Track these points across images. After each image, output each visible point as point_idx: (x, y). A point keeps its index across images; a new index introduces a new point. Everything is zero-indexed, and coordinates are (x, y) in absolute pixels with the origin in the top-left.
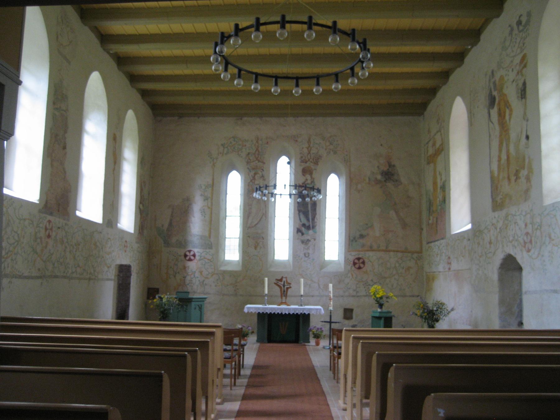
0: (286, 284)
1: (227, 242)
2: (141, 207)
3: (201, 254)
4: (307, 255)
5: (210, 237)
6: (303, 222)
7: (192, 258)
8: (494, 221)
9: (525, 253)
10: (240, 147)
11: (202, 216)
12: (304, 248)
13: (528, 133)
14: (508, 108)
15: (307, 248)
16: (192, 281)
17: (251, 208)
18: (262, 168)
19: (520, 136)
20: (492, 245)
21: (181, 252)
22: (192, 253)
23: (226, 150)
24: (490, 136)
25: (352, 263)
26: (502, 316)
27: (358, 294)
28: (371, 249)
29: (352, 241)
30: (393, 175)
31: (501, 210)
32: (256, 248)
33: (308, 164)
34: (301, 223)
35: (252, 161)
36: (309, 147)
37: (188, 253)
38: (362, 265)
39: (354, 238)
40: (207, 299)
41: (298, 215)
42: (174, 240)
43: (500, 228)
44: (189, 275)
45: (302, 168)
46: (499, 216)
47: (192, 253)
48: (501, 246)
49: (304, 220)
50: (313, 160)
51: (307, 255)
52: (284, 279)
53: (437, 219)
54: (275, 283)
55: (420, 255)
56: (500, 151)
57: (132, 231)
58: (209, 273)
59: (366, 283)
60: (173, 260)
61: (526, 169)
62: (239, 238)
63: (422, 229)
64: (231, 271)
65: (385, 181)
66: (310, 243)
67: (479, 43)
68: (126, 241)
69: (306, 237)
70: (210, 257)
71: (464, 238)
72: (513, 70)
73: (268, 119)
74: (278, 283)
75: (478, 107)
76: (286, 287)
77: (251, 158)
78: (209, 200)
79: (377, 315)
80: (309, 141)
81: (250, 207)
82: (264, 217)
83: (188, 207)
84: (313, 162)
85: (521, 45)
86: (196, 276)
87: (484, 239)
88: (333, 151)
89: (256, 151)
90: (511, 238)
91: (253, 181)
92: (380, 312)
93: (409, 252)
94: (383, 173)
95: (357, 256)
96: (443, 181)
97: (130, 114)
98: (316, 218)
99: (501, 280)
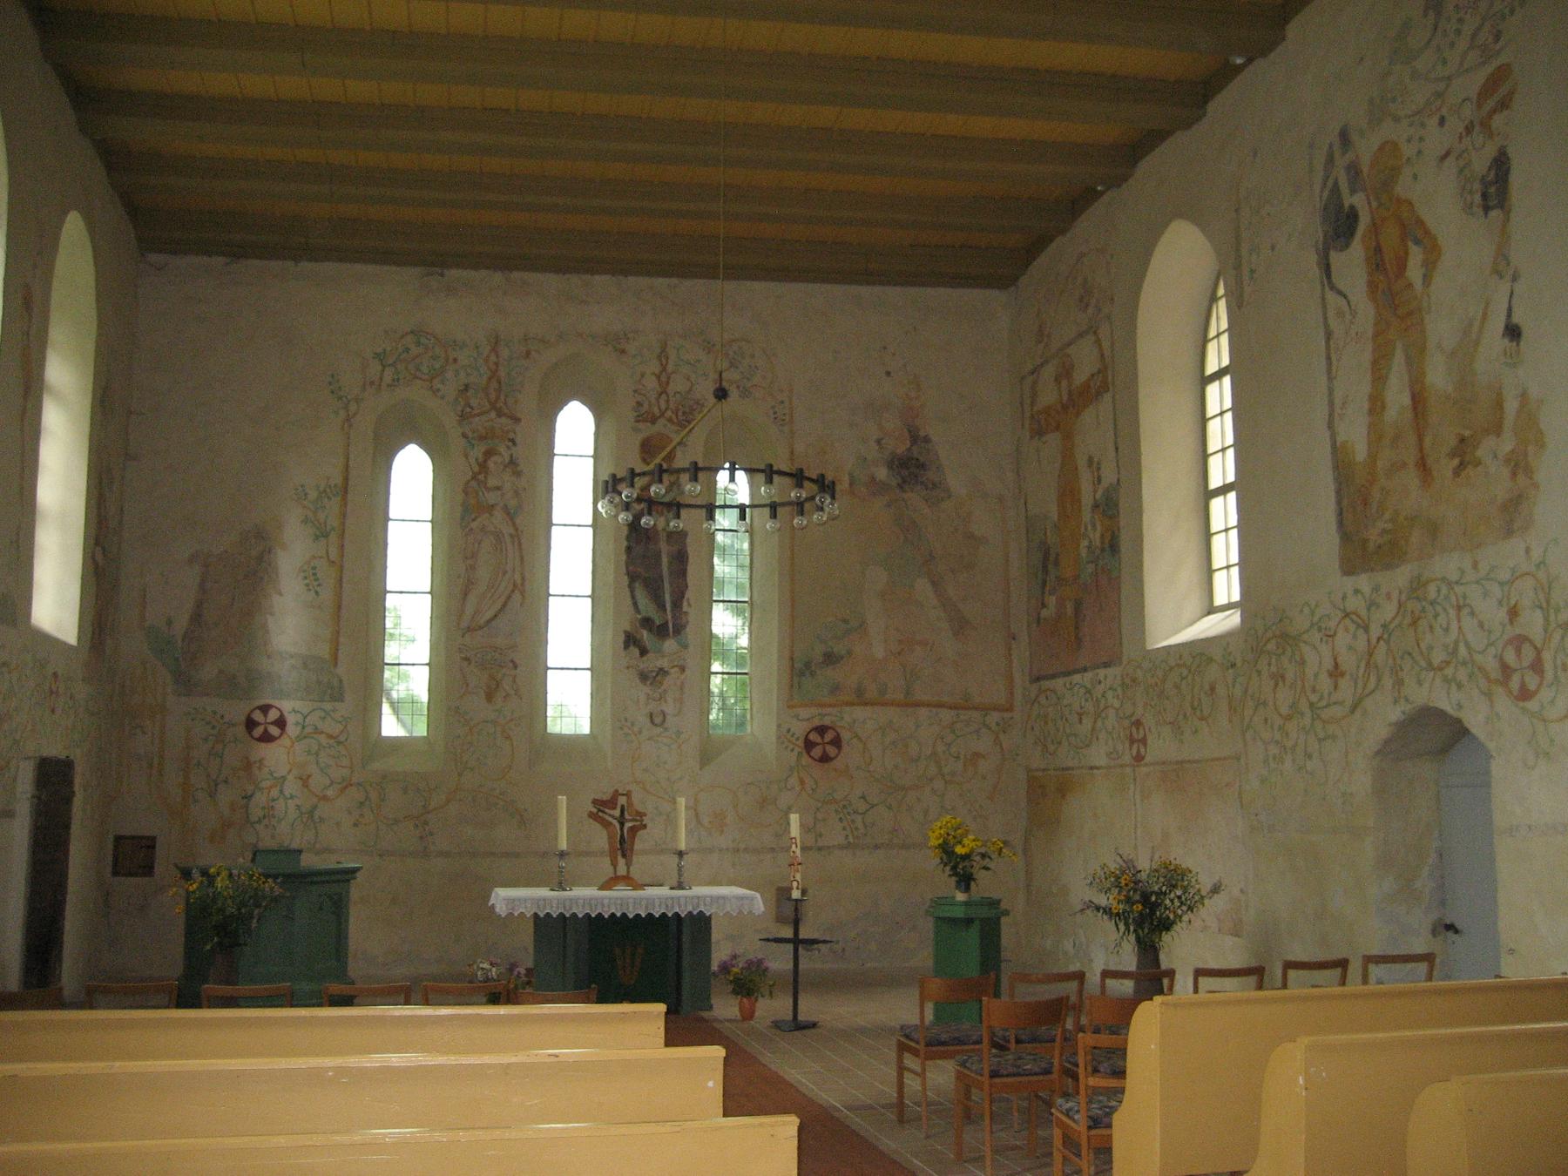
0: (627, 816)
2: (99, 558)
3: (305, 717)
6: (644, 614)
7: (274, 731)
8: (1354, 603)
9: (1503, 704)
13: (1515, 319)
14: (1417, 242)
15: (657, 695)
17: (473, 568)
18: (511, 435)
19: (1475, 328)
20: (1344, 683)
21: (237, 711)
22: (273, 715)
24: (1329, 335)
25: (801, 743)
27: (820, 844)
28: (861, 699)
31: (1388, 567)
32: (490, 697)
33: (659, 427)
34: (639, 617)
35: (476, 412)
36: (661, 373)
37: (258, 716)
38: (831, 750)
39: (807, 665)
40: (358, 875)
42: (208, 671)
44: (261, 789)
45: (640, 437)
46: (1376, 589)
47: (273, 715)
49: (647, 607)
50: (677, 415)
51: (656, 720)
52: (622, 800)
53: (1078, 605)
54: (591, 815)
55: (1007, 715)
56: (1379, 377)
57: (70, 634)
61: (1507, 434)
65: (900, 486)
66: (668, 682)
68: (55, 675)
69: (652, 663)
70: (335, 729)
71: (1211, 660)
72: (1442, 121)
76: (628, 825)
77: (474, 402)
78: (333, 537)
79: (959, 913)
80: (663, 355)
81: (469, 562)
82: (517, 596)
83: (260, 559)
86: (287, 794)
88: (738, 387)
92: (966, 904)
95: (817, 722)
96: (1105, 483)
97: (74, 228)
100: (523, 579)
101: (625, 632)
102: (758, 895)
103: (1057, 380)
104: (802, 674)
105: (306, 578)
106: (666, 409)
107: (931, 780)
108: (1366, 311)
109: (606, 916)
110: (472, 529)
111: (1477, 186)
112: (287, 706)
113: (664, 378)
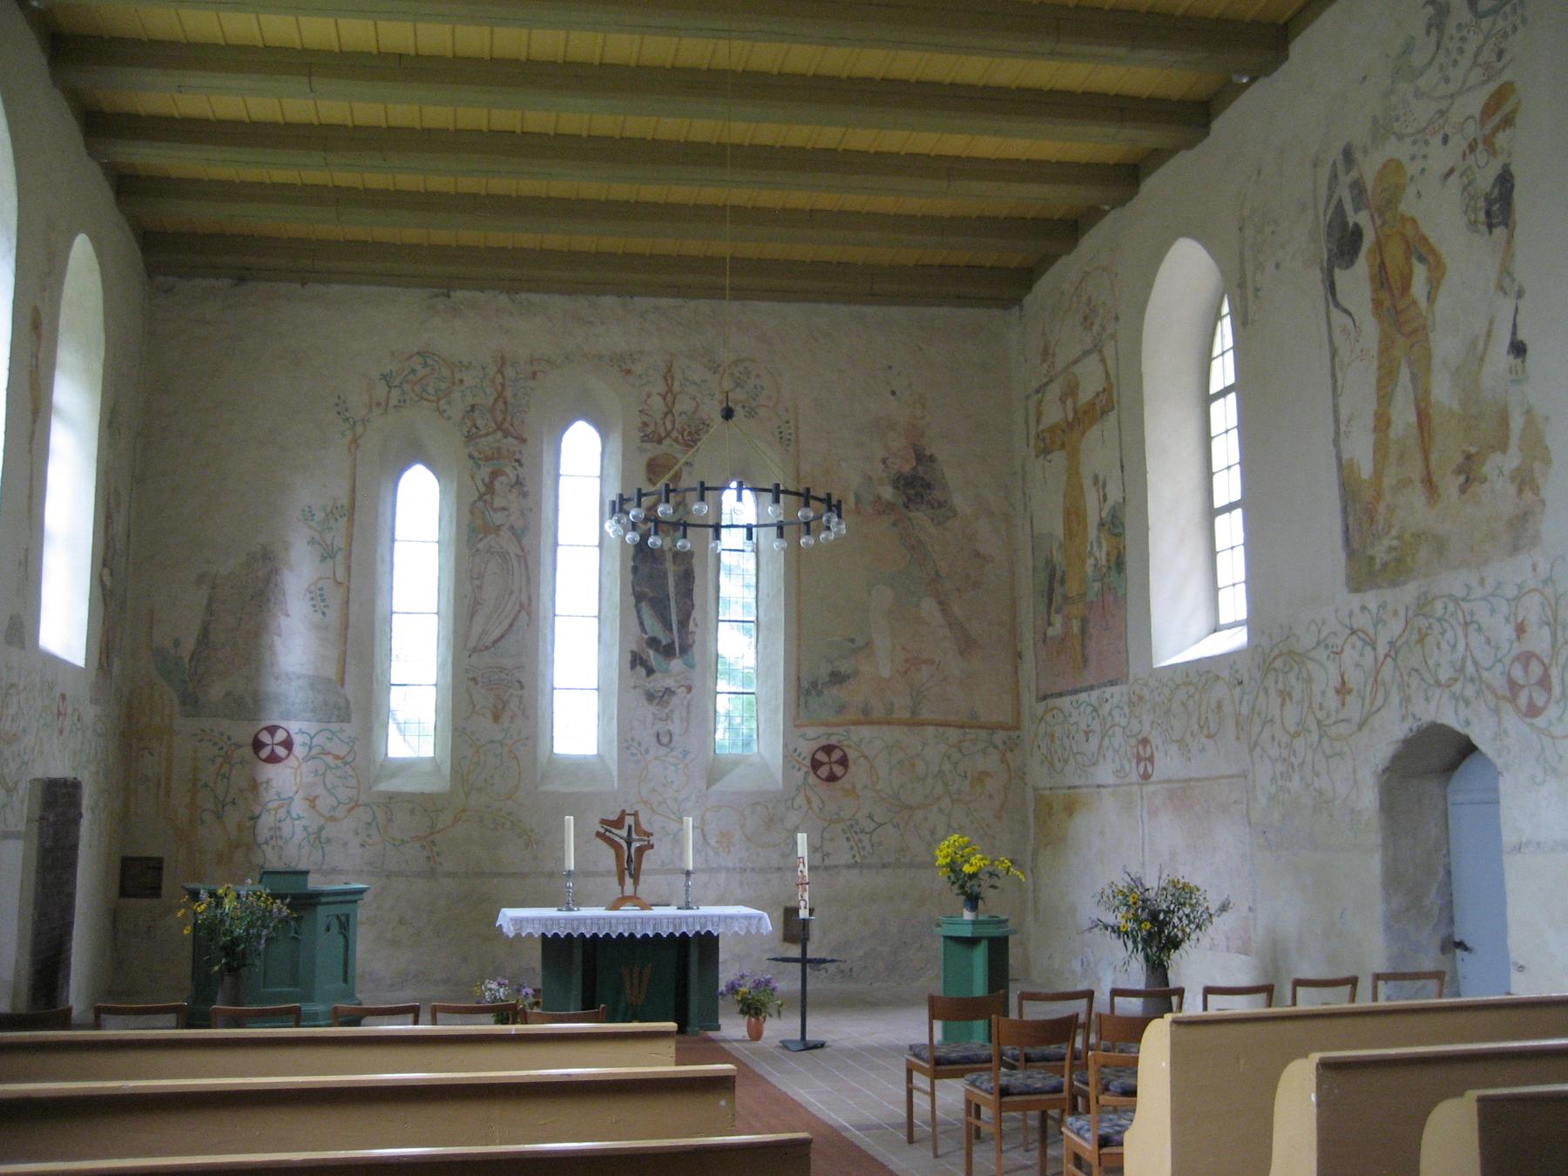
0: (634, 836)
1: (396, 698)
2: (107, 579)
4: (663, 739)
5: (342, 683)
6: (650, 634)
7: (281, 751)
8: (1361, 621)
9: (1511, 721)
10: (444, 386)
11: (316, 611)
12: (654, 715)
13: (1521, 336)
14: (1422, 259)
15: (663, 716)
16: (279, 828)
17: (480, 587)
18: (517, 456)
19: (1481, 346)
20: (1351, 700)
21: (243, 733)
22: (280, 736)
23: (395, 393)
24: (1334, 353)
25: (808, 762)
26: (1394, 924)
27: (827, 862)
28: (866, 718)
29: (808, 692)
30: (928, 486)
32: (496, 717)
33: (666, 446)
34: (646, 637)
37: (265, 737)
38: (838, 770)
39: (814, 685)
41: (634, 610)
42: (216, 692)
43: (1391, 644)
46: (1383, 606)
47: (280, 736)
48: (1395, 699)
49: (654, 628)
52: (629, 820)
54: (598, 834)
55: (1014, 734)
58: (339, 803)
59: (852, 826)
60: (213, 761)
62: (436, 685)
63: (1020, 656)
64: (414, 795)
66: (675, 700)
67: (1285, 67)
68: (63, 697)
69: (659, 682)
70: (342, 750)
71: (1217, 678)
72: (1445, 140)
73: (535, 298)
74: (607, 833)
75: (1277, 266)
76: (636, 845)
77: (480, 423)
78: (340, 557)
79: (967, 932)
80: (668, 376)
81: (477, 582)
83: (267, 580)
84: (681, 440)
85: (1488, 55)
87: (1309, 681)
88: (743, 407)
89: (496, 400)
90: (1445, 674)
91: (488, 497)
92: (974, 923)
93: (981, 727)
94: (898, 479)
95: (824, 742)
97: (82, 249)
98: (692, 618)
99: (1391, 804)
100: (530, 598)
101: (632, 652)
102: (765, 915)
103: (1063, 400)
104: (808, 692)
105: (313, 599)
106: (673, 429)
107: (938, 799)
108: (1370, 328)
109: (614, 937)
110: (478, 550)
111: (1481, 203)
112: (294, 726)
113: (669, 396)
